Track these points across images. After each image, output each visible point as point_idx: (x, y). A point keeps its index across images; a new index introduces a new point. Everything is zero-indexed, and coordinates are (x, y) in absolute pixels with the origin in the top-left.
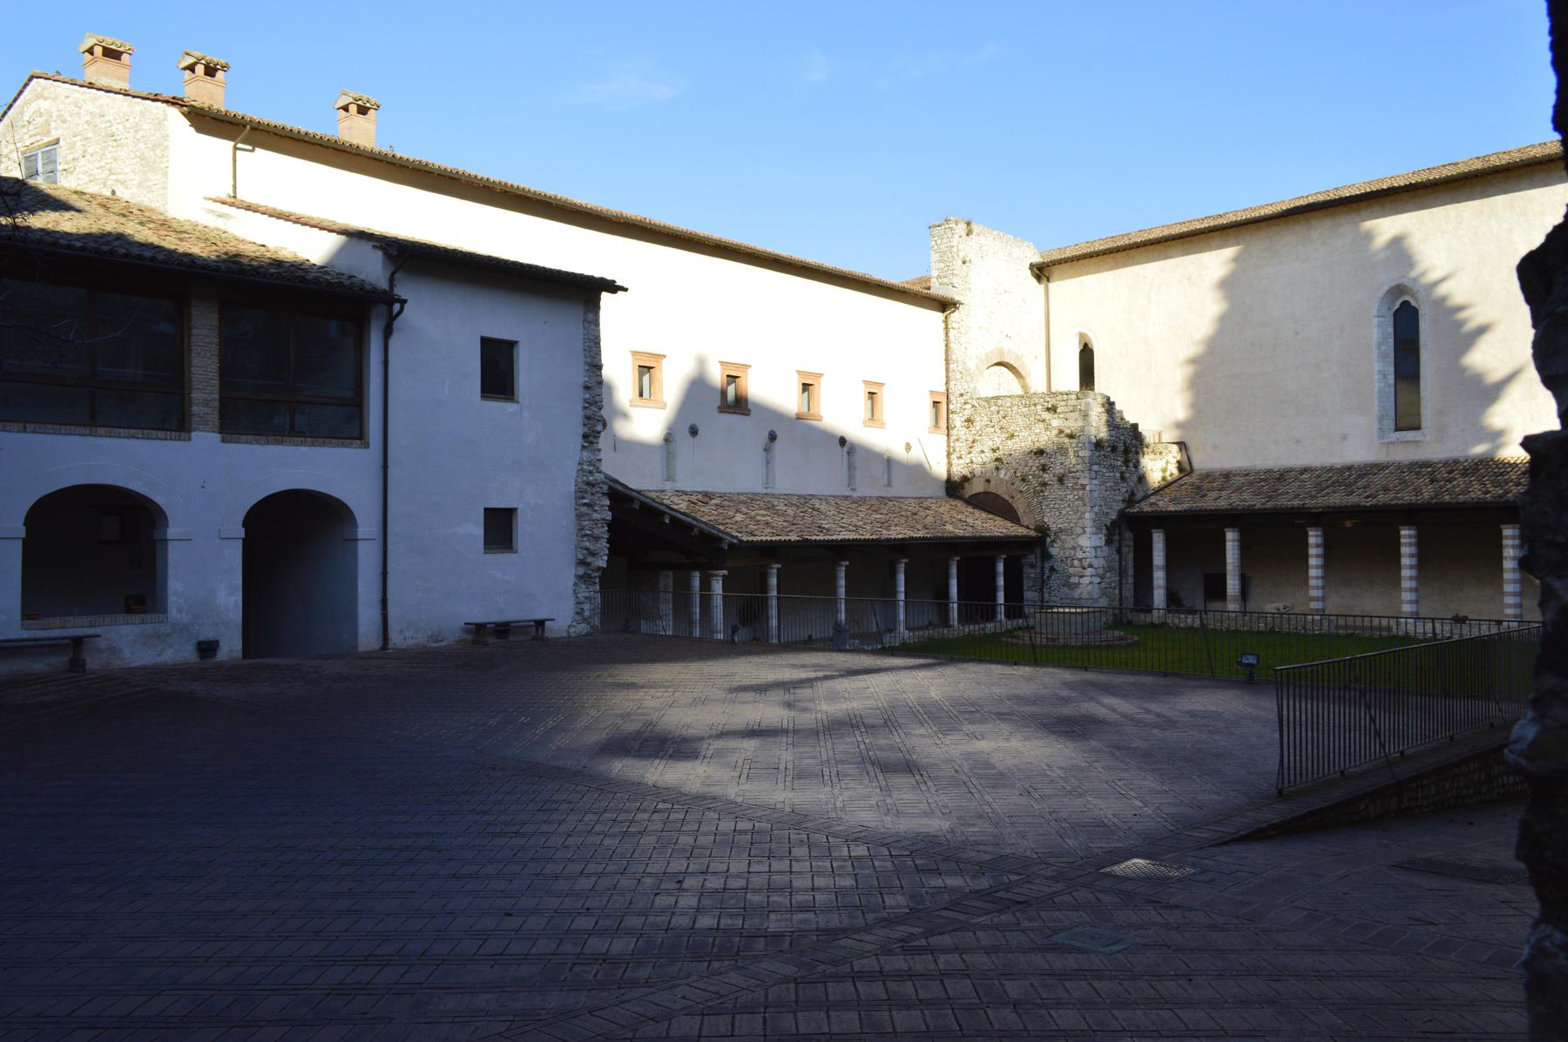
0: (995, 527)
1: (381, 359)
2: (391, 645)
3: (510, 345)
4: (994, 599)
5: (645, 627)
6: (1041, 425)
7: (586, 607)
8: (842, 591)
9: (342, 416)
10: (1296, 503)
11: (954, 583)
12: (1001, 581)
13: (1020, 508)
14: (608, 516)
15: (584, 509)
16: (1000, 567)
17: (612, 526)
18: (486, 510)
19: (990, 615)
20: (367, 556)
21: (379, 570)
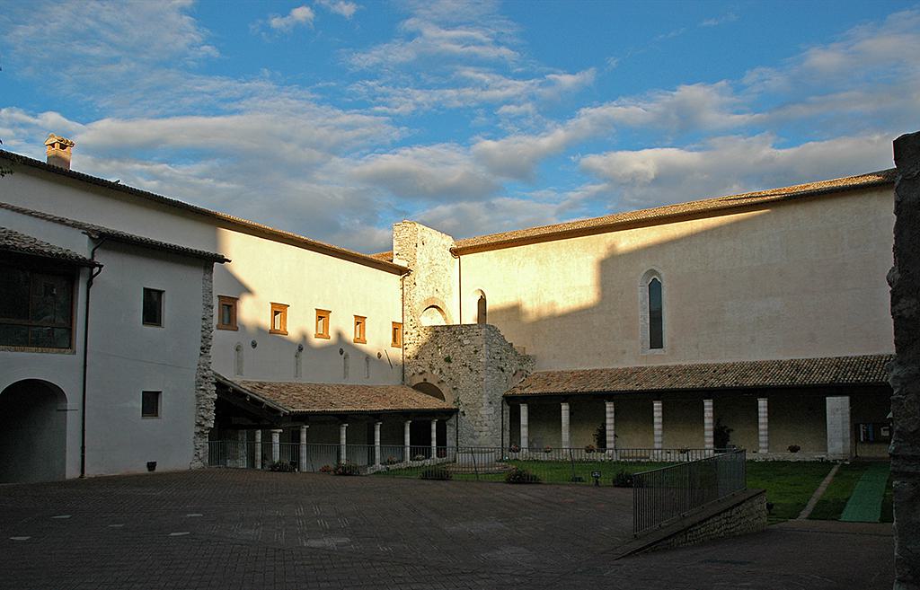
0: (431, 403)
1: (85, 300)
2: (86, 475)
3: (160, 293)
4: (430, 444)
5: (229, 463)
6: (457, 343)
7: (201, 452)
8: (343, 441)
9: (58, 335)
10: (599, 389)
11: (408, 436)
12: (434, 435)
13: (445, 390)
14: (215, 396)
15: (201, 392)
16: (434, 427)
17: (217, 402)
18: (144, 392)
19: (428, 456)
20: (73, 420)
21: (80, 430)
